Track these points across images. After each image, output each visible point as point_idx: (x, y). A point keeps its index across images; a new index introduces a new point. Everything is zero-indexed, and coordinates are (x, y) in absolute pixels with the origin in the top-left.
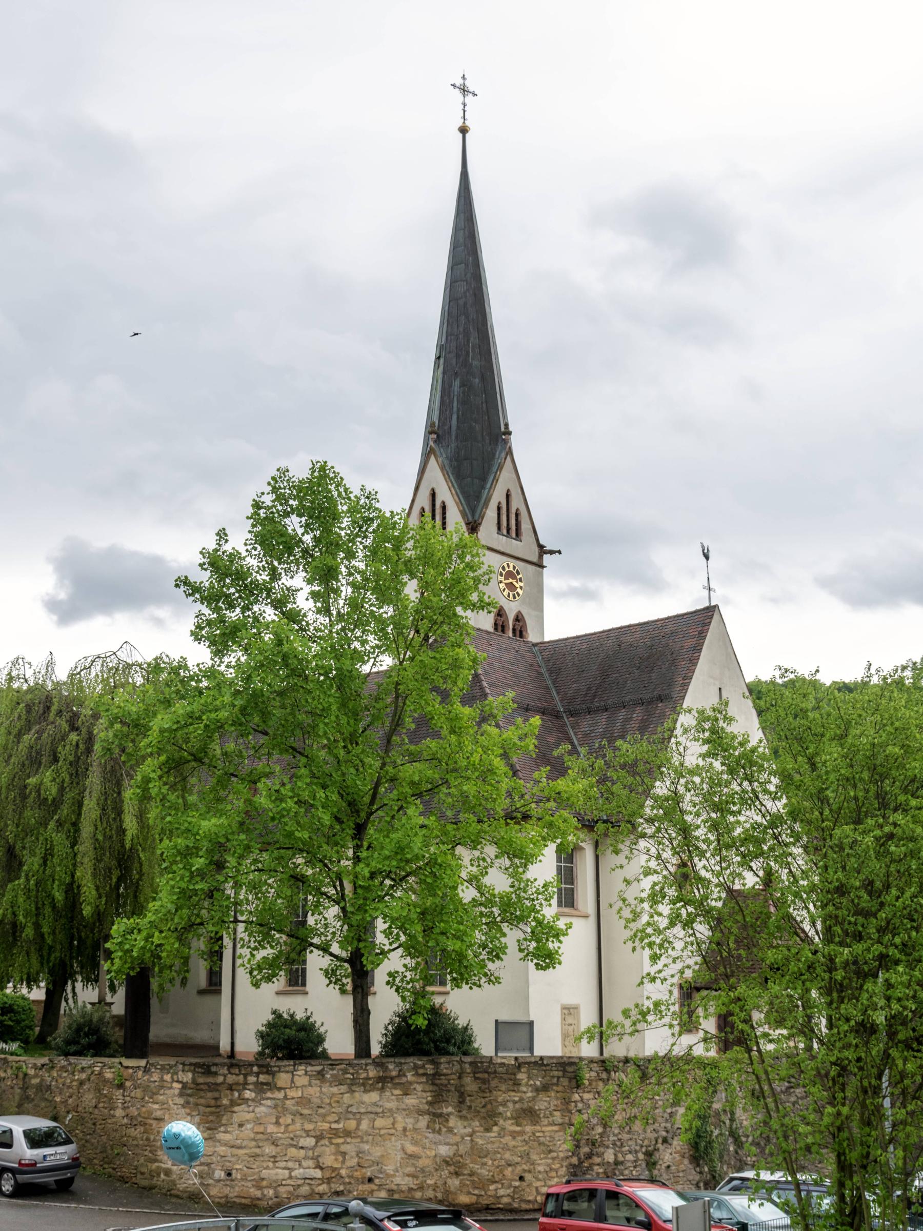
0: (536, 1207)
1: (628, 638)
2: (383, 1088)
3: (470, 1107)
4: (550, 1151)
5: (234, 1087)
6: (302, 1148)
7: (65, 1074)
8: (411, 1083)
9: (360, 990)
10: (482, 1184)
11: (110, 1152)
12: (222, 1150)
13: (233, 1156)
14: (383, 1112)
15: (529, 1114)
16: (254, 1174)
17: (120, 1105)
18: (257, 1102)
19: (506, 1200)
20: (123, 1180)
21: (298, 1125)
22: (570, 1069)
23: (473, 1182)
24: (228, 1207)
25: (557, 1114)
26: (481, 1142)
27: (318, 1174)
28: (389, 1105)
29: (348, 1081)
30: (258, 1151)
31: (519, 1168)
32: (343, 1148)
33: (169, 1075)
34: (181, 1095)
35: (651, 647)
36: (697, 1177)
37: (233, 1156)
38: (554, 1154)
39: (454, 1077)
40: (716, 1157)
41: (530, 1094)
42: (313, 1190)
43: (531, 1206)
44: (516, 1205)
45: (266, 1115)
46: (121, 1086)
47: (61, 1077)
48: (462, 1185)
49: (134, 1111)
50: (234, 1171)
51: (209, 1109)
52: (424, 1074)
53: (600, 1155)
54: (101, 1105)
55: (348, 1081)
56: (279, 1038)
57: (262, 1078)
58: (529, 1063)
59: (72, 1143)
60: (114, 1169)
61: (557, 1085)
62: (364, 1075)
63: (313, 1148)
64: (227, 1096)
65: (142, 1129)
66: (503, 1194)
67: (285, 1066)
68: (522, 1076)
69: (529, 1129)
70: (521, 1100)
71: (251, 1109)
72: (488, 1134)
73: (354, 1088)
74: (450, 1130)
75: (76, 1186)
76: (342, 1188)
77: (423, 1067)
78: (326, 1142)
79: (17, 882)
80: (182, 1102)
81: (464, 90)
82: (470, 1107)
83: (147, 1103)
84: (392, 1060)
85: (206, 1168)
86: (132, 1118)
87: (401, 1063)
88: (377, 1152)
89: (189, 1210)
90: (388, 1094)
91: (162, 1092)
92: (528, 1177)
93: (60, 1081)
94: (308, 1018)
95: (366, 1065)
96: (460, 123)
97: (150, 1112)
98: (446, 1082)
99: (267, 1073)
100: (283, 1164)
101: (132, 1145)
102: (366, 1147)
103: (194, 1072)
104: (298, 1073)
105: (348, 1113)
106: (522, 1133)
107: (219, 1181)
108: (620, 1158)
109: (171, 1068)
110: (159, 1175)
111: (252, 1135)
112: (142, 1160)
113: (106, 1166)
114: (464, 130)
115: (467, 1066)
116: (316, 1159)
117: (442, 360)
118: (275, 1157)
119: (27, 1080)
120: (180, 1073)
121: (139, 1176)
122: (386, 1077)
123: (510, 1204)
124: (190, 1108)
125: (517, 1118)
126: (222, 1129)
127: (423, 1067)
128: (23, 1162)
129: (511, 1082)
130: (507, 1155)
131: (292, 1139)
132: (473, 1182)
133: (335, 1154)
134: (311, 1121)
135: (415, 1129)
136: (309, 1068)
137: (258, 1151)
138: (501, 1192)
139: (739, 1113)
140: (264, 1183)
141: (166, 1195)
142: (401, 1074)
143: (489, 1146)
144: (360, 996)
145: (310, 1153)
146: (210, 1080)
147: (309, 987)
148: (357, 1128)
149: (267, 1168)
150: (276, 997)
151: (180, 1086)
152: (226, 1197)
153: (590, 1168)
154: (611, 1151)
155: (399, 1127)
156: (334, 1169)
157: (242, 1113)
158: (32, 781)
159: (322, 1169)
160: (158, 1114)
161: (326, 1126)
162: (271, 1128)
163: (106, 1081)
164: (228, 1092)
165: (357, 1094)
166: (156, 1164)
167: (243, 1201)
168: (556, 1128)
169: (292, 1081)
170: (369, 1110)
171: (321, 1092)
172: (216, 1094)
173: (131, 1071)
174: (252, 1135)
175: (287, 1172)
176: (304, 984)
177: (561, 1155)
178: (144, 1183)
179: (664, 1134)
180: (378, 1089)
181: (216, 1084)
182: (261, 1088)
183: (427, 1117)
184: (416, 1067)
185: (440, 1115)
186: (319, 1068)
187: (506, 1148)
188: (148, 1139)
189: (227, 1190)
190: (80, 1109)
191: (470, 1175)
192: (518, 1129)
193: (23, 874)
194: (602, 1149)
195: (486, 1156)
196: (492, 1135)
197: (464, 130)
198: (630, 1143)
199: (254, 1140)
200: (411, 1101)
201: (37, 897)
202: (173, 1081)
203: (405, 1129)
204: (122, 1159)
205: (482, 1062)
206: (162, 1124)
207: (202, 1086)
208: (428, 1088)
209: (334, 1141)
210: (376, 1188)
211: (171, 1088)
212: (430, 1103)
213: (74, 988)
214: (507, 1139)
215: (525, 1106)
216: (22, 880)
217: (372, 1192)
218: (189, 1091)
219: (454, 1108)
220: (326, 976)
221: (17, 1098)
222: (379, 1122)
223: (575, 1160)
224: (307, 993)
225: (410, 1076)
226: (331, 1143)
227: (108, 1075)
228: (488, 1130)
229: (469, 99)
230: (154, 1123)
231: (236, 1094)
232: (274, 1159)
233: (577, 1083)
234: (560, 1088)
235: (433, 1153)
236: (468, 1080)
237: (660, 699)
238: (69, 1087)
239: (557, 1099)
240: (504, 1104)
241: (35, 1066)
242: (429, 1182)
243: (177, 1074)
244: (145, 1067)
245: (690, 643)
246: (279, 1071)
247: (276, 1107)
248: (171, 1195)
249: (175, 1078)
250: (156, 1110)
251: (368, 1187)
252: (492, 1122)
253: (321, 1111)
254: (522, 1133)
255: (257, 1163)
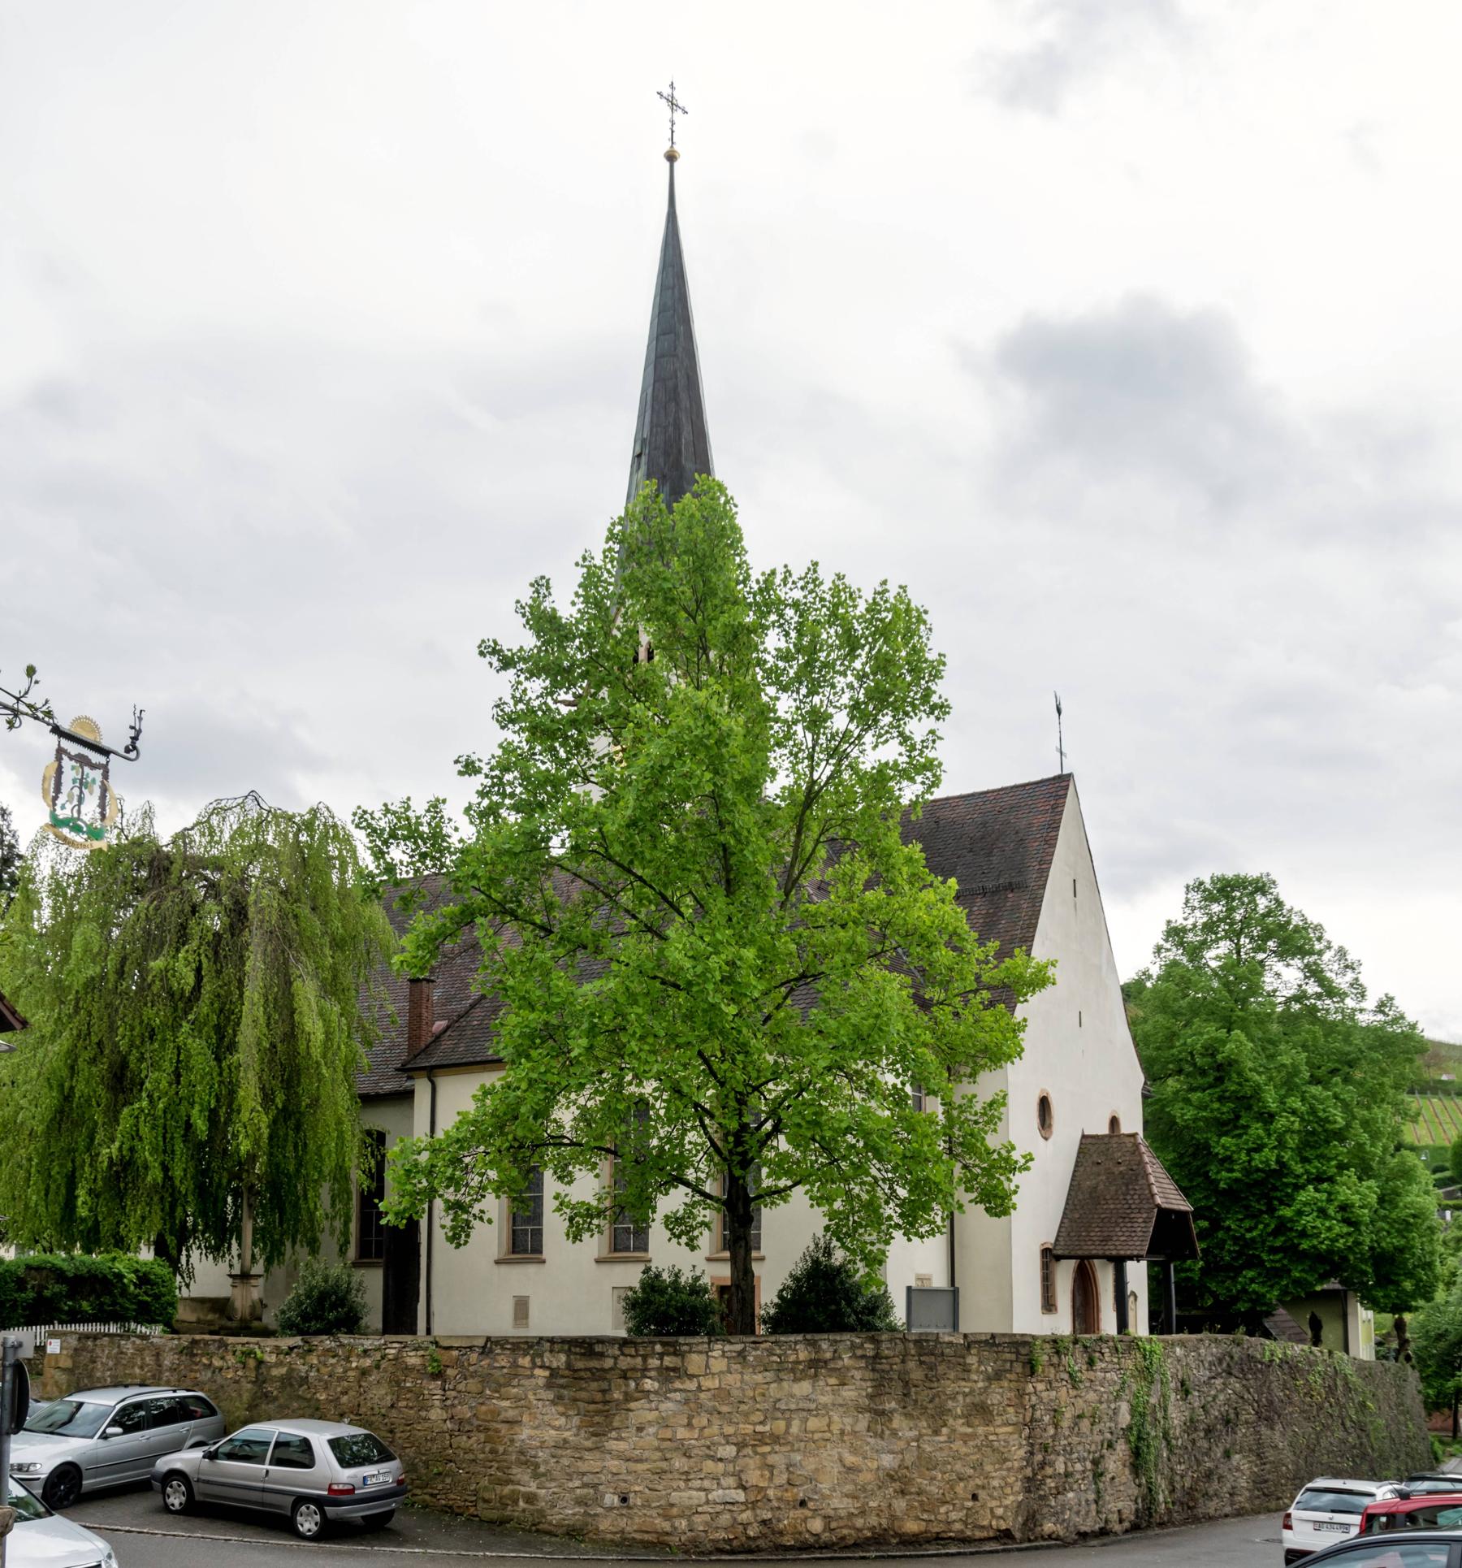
0: (991, 1534)
1: (948, 813)
2: (816, 1375)
3: (916, 1401)
4: (1006, 1460)
5: (629, 1374)
6: (721, 1460)
7: (333, 1361)
8: (848, 1369)
9: (743, 1244)
10: (929, 1506)
11: (424, 1471)
12: (613, 1464)
13: (629, 1473)
14: (817, 1409)
15: (981, 1411)
16: (659, 1498)
17: (437, 1403)
18: (663, 1395)
19: (958, 1526)
20: (451, 1511)
21: (715, 1429)
22: (1023, 1351)
23: (921, 1503)
24: (625, 1545)
25: (1011, 1410)
26: (929, 1449)
27: (740, 1496)
28: (823, 1399)
29: (775, 1366)
30: (664, 1465)
31: (972, 1483)
32: (771, 1459)
33: (528, 1358)
34: (549, 1386)
35: (984, 824)
36: (1136, 1492)
37: (629, 1473)
38: (1009, 1464)
39: (897, 1360)
40: (1151, 1466)
41: (980, 1384)
42: (735, 1519)
43: (985, 1534)
44: (969, 1533)
45: (675, 1414)
46: (438, 1375)
47: (325, 1365)
48: (910, 1507)
49: (464, 1411)
50: (632, 1495)
51: (592, 1407)
52: (863, 1357)
53: (1052, 1464)
54: (402, 1404)
55: (775, 1366)
56: (669, 1306)
57: (668, 1361)
58: (980, 1342)
59: (394, 1459)
60: (432, 1495)
61: (1010, 1371)
62: (792, 1358)
63: (734, 1460)
64: (618, 1387)
65: (482, 1436)
66: (953, 1517)
67: (697, 1344)
68: (972, 1360)
69: (981, 1430)
70: (972, 1391)
71: (653, 1405)
72: (937, 1438)
73: (782, 1375)
74: (894, 1433)
75: (393, 1524)
76: (769, 1516)
77: (861, 1346)
78: (749, 1451)
79: (137, 1105)
80: (551, 1396)
81: (673, 104)
82: (916, 1401)
83: (491, 1398)
84: (825, 1336)
85: (592, 1491)
86: (461, 1421)
87: (836, 1341)
88: (810, 1464)
89: (577, 1552)
90: (822, 1383)
91: (515, 1382)
92: (982, 1494)
93: (324, 1370)
94: (697, 1279)
95: (796, 1343)
96: (667, 147)
97: (496, 1413)
98: (887, 1367)
99: (675, 1354)
100: (697, 1484)
101: (463, 1461)
102: (798, 1457)
103: (569, 1353)
104: (714, 1354)
105: (774, 1411)
106: (974, 1436)
107: (611, 1509)
108: (1070, 1469)
109: (531, 1347)
110: (516, 1502)
111: (656, 1443)
112: (485, 1482)
113: (418, 1491)
114: (671, 157)
115: (911, 1345)
116: (737, 1475)
117: (644, 459)
118: (687, 1473)
119: (263, 1370)
120: (547, 1354)
121: (481, 1505)
122: (819, 1360)
123: (962, 1531)
124: (565, 1405)
125: (967, 1418)
126: (614, 1434)
127: (861, 1346)
128: (335, 1487)
129: (959, 1368)
130: (958, 1467)
131: (708, 1447)
132: (921, 1503)
133: (759, 1468)
134: (731, 1422)
135: (855, 1432)
136: (728, 1347)
137: (664, 1465)
138: (953, 1516)
139: (1171, 1408)
140: (675, 1511)
141: (530, 1531)
142: (836, 1356)
143: (938, 1454)
144: (742, 1252)
145: (730, 1468)
146: (594, 1364)
147: (547, 1252)
148: (787, 1432)
149: (678, 1489)
150: (496, 1267)
151: (547, 1373)
152: (622, 1532)
153: (1043, 1482)
154: (1061, 1459)
155: (835, 1429)
156: (761, 1489)
157: (641, 1412)
158: (157, 964)
159: (744, 1488)
160: (511, 1414)
161: (749, 1429)
162: (682, 1433)
163: (408, 1369)
164: (621, 1381)
165: (785, 1384)
166: (510, 1487)
167: (646, 1537)
168: (1010, 1429)
169: (707, 1366)
170: (801, 1405)
171: (742, 1381)
172: (604, 1385)
173: (455, 1353)
174: (656, 1443)
175: (703, 1494)
176: (538, 1249)
177: (1016, 1464)
178: (494, 1515)
179: (1109, 1436)
180: (811, 1377)
181: (603, 1370)
182: (668, 1375)
183: (867, 1415)
184: (853, 1347)
185: (883, 1413)
186: (739, 1347)
187: (957, 1457)
188: (493, 1451)
189: (622, 1523)
190: (363, 1410)
191: (918, 1494)
192: (970, 1430)
193: (144, 1095)
194: (1053, 1457)
195: (935, 1468)
196: (942, 1439)
197: (671, 157)
198: (1080, 1448)
199: (658, 1449)
200: (848, 1393)
201: (165, 1128)
202: (534, 1366)
203: (842, 1432)
204: (448, 1480)
205: (927, 1341)
206: (517, 1429)
207: (582, 1374)
208: (869, 1375)
209: (759, 1450)
210: (809, 1514)
211: (532, 1376)
212: (871, 1397)
213: (188, 1256)
214: (958, 1445)
215: (977, 1400)
216: (145, 1103)
217: (805, 1520)
218: (562, 1381)
219: (898, 1402)
220: (667, 1227)
221: (246, 1397)
222: (813, 1423)
223: (1029, 1472)
224: (544, 1262)
225: (847, 1360)
226: (756, 1453)
227: (413, 1359)
228: (936, 1433)
229: (678, 114)
230: (504, 1428)
231: (633, 1384)
232: (686, 1476)
233: (1031, 1368)
234: (1013, 1377)
235: (875, 1465)
236: (911, 1365)
237: (1010, 887)
238: (340, 1379)
239: (1010, 1389)
240: (953, 1398)
241: (278, 1350)
242: (872, 1504)
243: (541, 1356)
244: (484, 1347)
245: (1040, 820)
246: (690, 1352)
247: (687, 1402)
248: (537, 1531)
249: (538, 1361)
250: (506, 1409)
251: (801, 1512)
252: (940, 1422)
253: (743, 1407)
254: (974, 1436)
255: (664, 1483)
